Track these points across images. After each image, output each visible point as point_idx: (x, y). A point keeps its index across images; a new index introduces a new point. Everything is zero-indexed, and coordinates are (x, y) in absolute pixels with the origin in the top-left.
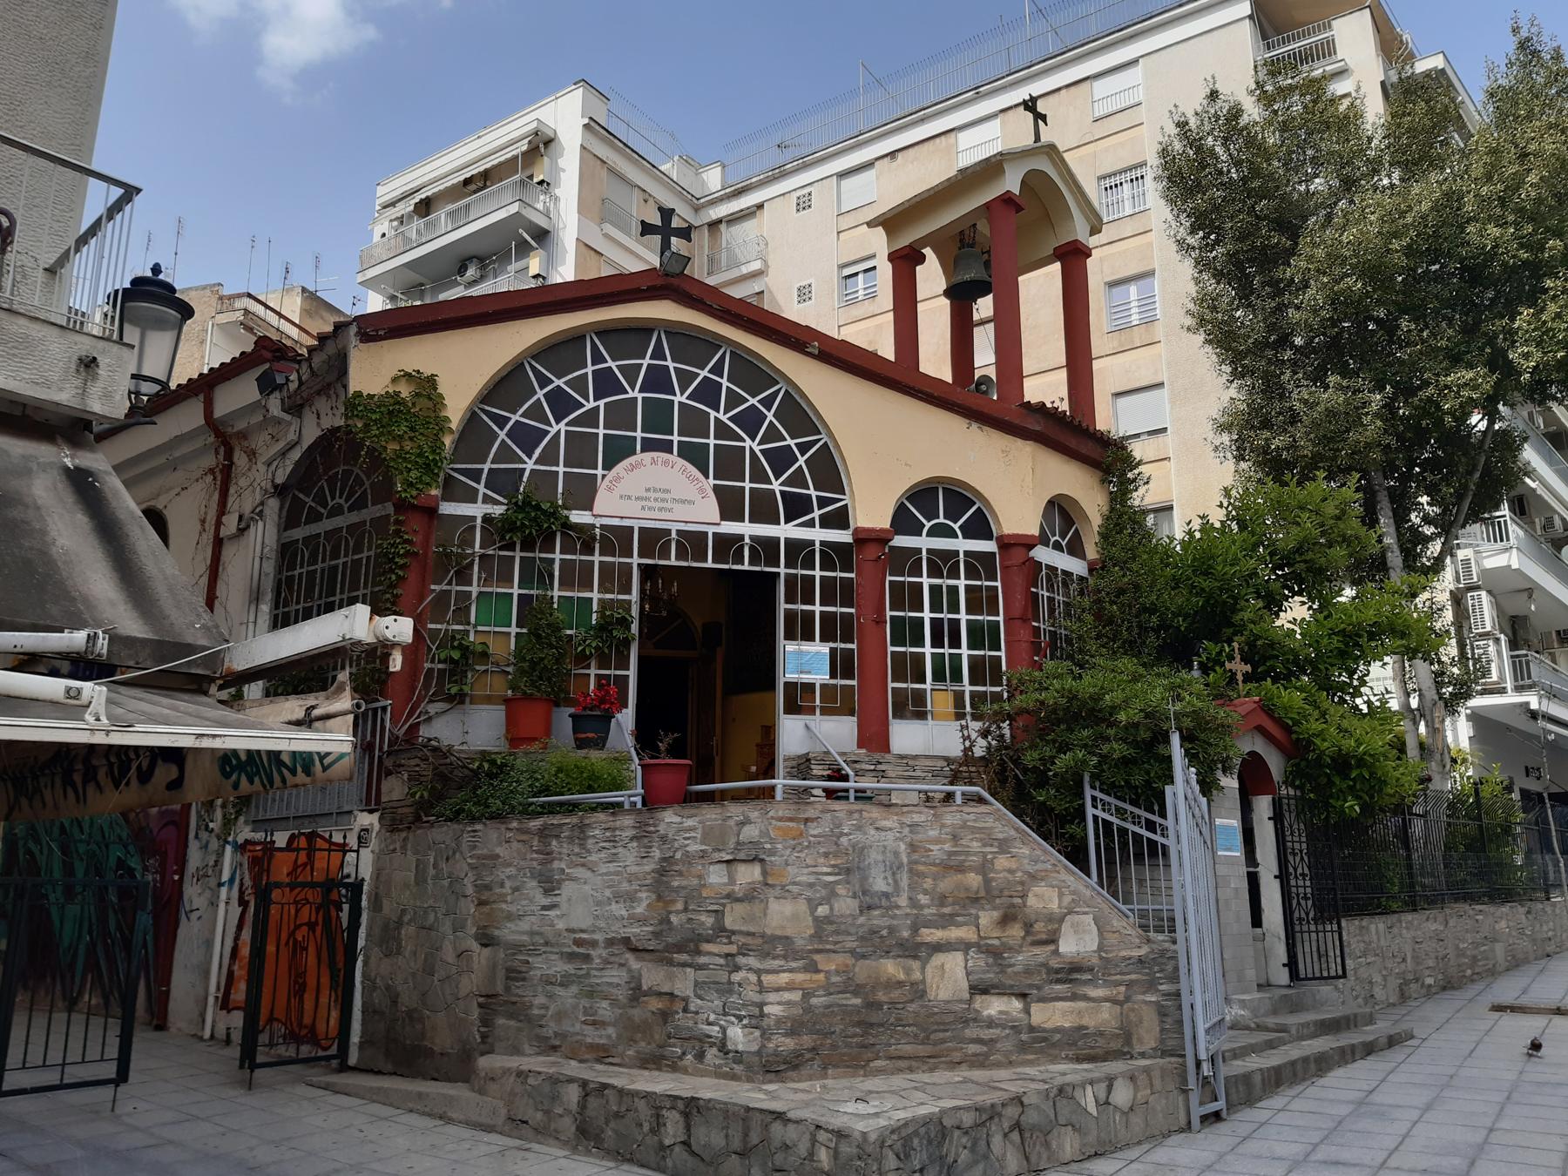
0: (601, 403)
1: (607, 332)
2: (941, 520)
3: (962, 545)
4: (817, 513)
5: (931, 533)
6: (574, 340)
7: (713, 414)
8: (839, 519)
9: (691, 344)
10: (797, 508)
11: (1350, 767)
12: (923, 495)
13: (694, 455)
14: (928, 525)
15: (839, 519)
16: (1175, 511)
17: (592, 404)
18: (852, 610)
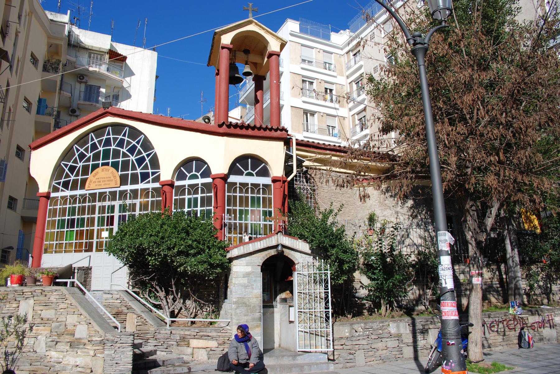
0: (92, 154)
1: (95, 130)
2: (194, 173)
3: (200, 181)
4: (151, 178)
5: (190, 178)
6: (86, 134)
7: (122, 150)
8: (157, 179)
9: (118, 128)
10: (145, 177)
11: (490, 240)
12: (187, 163)
13: (115, 165)
14: (189, 175)
15: (157, 179)
16: (127, 321)
17: (89, 155)
18: (161, 199)
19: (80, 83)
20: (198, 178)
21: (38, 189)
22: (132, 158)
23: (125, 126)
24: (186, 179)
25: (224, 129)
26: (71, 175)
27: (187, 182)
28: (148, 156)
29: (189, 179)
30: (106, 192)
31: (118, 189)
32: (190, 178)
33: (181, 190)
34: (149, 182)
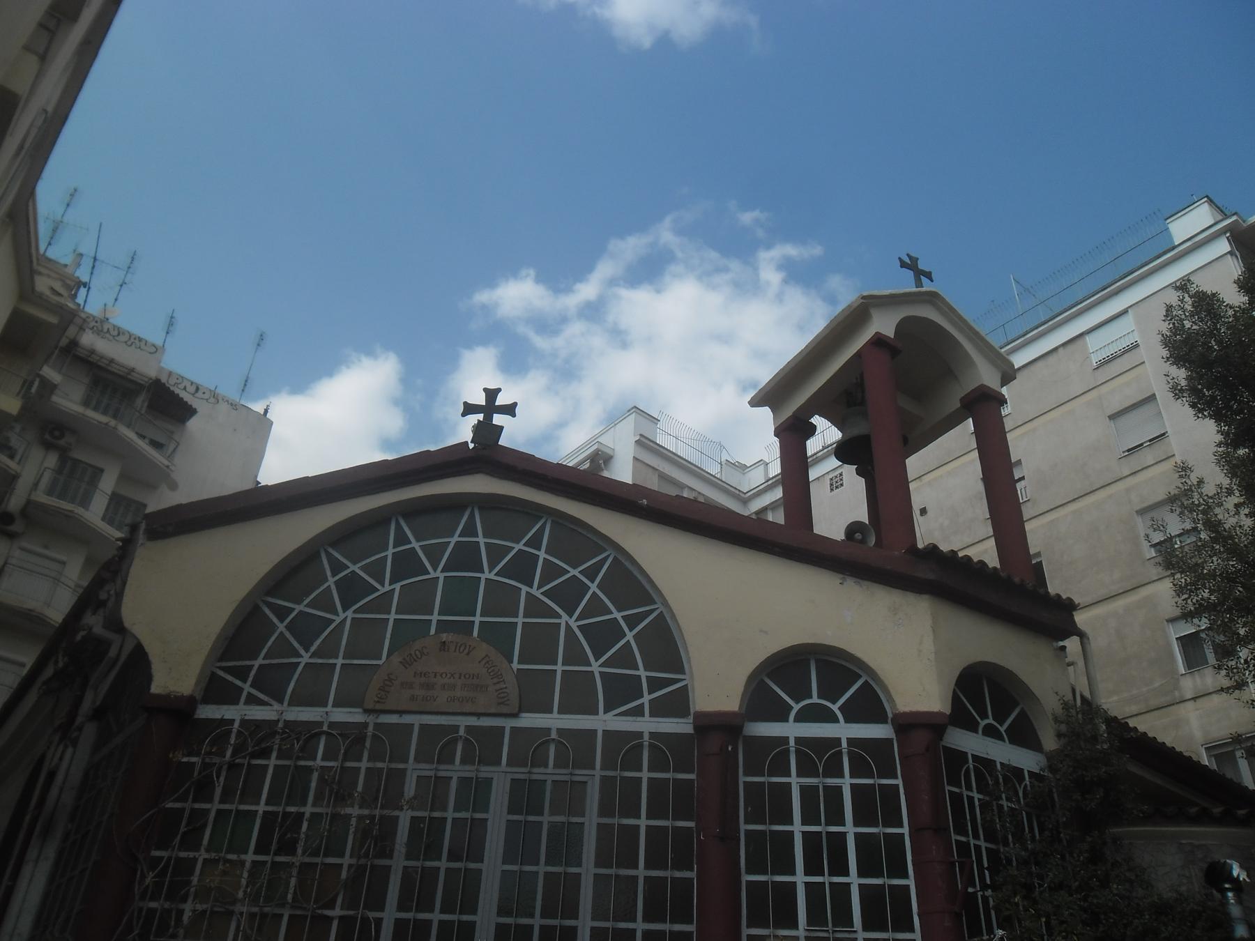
0: (397, 586)
2: (815, 699)
3: (844, 731)
4: (646, 699)
14: (796, 707)
17: (387, 588)
19: (48, 446)
20: (834, 720)
21: (149, 678)
22: (568, 622)
23: (537, 511)
24: (237, 704)
25: (924, 572)
26: (302, 652)
27: (791, 730)
28: (632, 621)
29: (797, 720)
30: (456, 728)
31: (509, 724)
32: (802, 717)
33: (772, 755)
34: (638, 712)
